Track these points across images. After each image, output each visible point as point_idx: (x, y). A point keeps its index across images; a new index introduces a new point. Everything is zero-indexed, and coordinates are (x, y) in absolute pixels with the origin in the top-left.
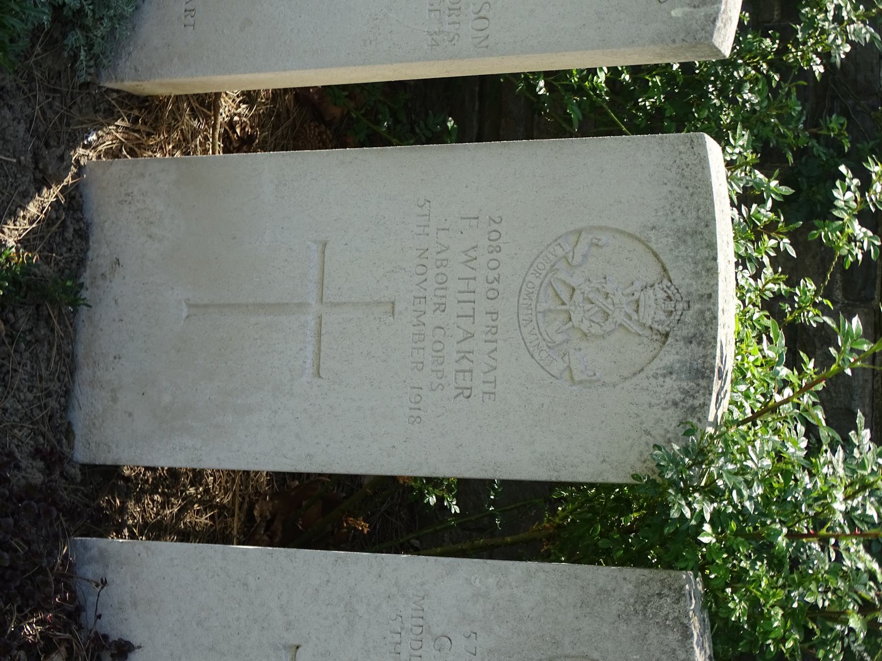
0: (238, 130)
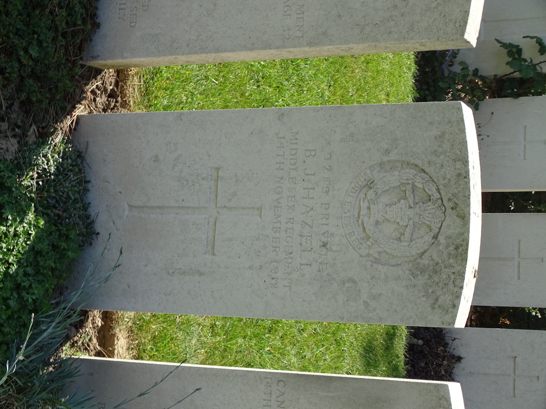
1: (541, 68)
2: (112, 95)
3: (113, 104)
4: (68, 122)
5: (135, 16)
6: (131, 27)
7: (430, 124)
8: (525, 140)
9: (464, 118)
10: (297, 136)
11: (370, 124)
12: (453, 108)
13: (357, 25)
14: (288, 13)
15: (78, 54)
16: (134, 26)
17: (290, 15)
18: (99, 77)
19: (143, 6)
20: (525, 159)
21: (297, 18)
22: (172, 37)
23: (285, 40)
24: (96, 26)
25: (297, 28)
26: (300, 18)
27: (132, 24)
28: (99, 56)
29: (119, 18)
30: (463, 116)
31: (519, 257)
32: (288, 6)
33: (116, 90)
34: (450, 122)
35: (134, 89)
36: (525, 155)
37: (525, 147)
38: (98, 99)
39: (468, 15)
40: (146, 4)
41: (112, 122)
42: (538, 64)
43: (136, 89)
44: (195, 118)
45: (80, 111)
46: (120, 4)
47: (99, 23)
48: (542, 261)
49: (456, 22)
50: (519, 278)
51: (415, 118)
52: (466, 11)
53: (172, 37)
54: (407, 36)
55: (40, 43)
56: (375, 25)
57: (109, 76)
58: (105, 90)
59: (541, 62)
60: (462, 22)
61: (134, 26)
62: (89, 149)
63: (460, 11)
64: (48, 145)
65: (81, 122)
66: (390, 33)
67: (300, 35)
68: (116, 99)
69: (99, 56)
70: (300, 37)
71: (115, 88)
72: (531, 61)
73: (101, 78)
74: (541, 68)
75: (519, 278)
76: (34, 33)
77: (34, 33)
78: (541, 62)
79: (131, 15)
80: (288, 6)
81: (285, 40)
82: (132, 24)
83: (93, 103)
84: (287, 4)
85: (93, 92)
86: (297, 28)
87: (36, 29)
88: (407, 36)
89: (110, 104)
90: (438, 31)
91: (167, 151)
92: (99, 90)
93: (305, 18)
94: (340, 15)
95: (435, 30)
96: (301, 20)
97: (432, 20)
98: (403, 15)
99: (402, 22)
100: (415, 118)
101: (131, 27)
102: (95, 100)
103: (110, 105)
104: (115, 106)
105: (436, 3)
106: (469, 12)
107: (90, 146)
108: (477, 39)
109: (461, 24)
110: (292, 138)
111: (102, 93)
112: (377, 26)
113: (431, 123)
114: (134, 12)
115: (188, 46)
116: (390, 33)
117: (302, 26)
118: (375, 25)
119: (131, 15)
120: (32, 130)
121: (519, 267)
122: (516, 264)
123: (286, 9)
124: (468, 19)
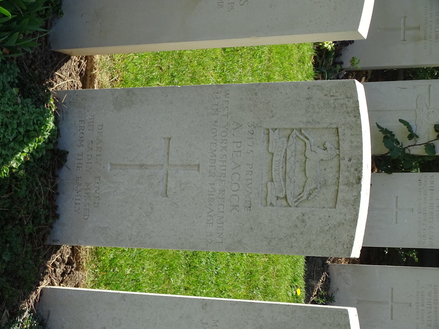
0: (30, 261)
1: (409, 151)
2: (70, 263)
3: (69, 270)
4: (34, 296)
5: (87, 211)
6: (85, 219)
7: (323, 325)
8: (397, 208)
9: (350, 323)
10: (217, 324)
11: (276, 320)
12: (341, 314)
13: (266, 238)
14: (210, 222)
15: (42, 244)
16: (87, 219)
17: (212, 223)
18: (59, 251)
19: (94, 203)
20: (397, 223)
21: (218, 227)
22: (117, 232)
23: (208, 243)
24: (57, 217)
25: (218, 235)
26: (220, 227)
27: (86, 217)
28: (59, 240)
29: (75, 211)
30: (349, 321)
31: (392, 301)
32: (211, 216)
33: (72, 259)
34: (339, 325)
35: (87, 251)
36: (397, 220)
37: (397, 214)
38: (57, 270)
39: (354, 239)
40: (97, 202)
41: (69, 296)
42: (407, 147)
43: (88, 252)
44: (136, 300)
45: (44, 284)
46: (76, 200)
47: (59, 215)
48: (411, 306)
49: (344, 244)
50: (392, 318)
51: (311, 318)
52: (352, 236)
53: (117, 232)
54: (305, 251)
55: (11, 248)
56: (280, 240)
57: (66, 250)
58: (63, 261)
59: (409, 146)
60: (349, 244)
61: (87, 219)
62: (50, 317)
63: (348, 235)
64: (17, 323)
65: (44, 293)
66: (292, 247)
67: (220, 241)
68: (72, 266)
69: (59, 240)
70: (220, 243)
71: (71, 257)
72: (402, 145)
73: (60, 252)
74: (409, 151)
75: (392, 318)
76: (7, 242)
77: (7, 242)
78: (409, 146)
79: (85, 209)
80: (211, 216)
81: (208, 243)
82: (86, 217)
83: (54, 274)
84: (210, 214)
85: (54, 265)
86: (218, 235)
87: (8, 239)
88: (305, 251)
89: (67, 270)
90: (330, 250)
91: (113, 325)
92: (58, 261)
93: (224, 227)
94: (252, 228)
95: (327, 249)
96: (221, 228)
97: (325, 240)
98: (302, 234)
99: (301, 239)
100: (311, 318)
101: (85, 219)
102: (55, 271)
103: (67, 271)
104: (71, 271)
105: (328, 227)
106: (354, 237)
107: (51, 314)
108: (361, 251)
109: (349, 247)
110: (214, 324)
111: (60, 264)
112: (282, 240)
113: (324, 324)
114: (87, 207)
115: (130, 239)
116: (292, 247)
117: (222, 234)
118: (280, 240)
119: (85, 209)
120: (5, 313)
121: (392, 310)
122: (390, 307)
123: (209, 218)
124: (353, 243)
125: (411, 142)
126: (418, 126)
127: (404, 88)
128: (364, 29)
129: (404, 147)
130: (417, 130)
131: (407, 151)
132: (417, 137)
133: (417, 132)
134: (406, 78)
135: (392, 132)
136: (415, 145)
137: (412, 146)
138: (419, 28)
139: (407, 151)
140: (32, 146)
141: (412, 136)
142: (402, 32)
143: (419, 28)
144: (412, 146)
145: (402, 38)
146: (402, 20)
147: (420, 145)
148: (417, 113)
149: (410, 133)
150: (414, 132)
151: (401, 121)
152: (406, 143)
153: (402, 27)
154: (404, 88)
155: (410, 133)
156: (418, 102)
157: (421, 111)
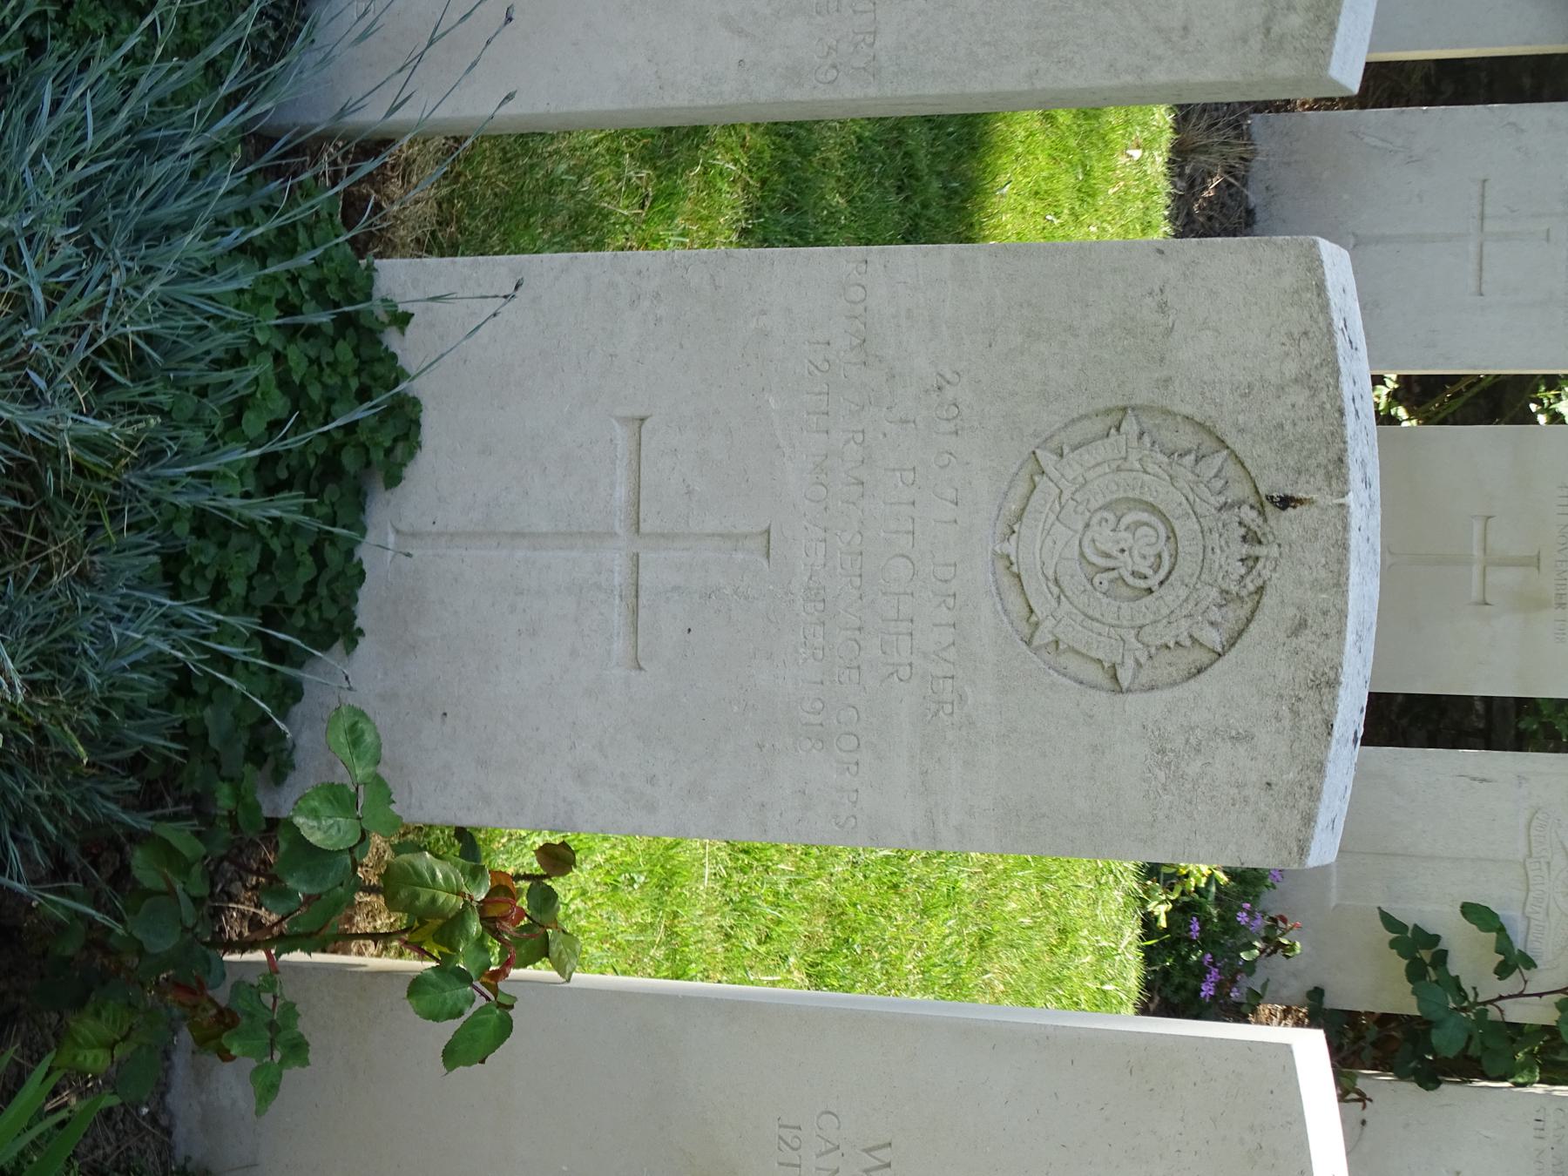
42: (1491, 1002)
59: (1501, 998)
72: (1477, 995)
78: (1501, 998)
125: (1511, 984)
126: (1533, 923)
127: (1483, 780)
128: (1324, 850)
129: (1480, 1000)
130: (1531, 937)
131: (1493, 1013)
132: (1530, 963)
133: (1529, 945)
134: (1488, 741)
135: (1437, 938)
136: (1521, 995)
137: (1510, 997)
138: (1536, 562)
139: (1493, 1013)
140: (93, 912)
141: (1512, 961)
142: (1476, 571)
143: (1536, 562)
144: (1510, 997)
145: (1476, 594)
146: (1477, 527)
147: (1540, 995)
148: (1531, 874)
149: (1502, 957)
150: (1519, 945)
151: (1469, 910)
152: (1490, 987)
153: (1477, 552)
154: (1483, 780)
155: (1502, 957)
156: (1533, 832)
157: (1544, 867)
